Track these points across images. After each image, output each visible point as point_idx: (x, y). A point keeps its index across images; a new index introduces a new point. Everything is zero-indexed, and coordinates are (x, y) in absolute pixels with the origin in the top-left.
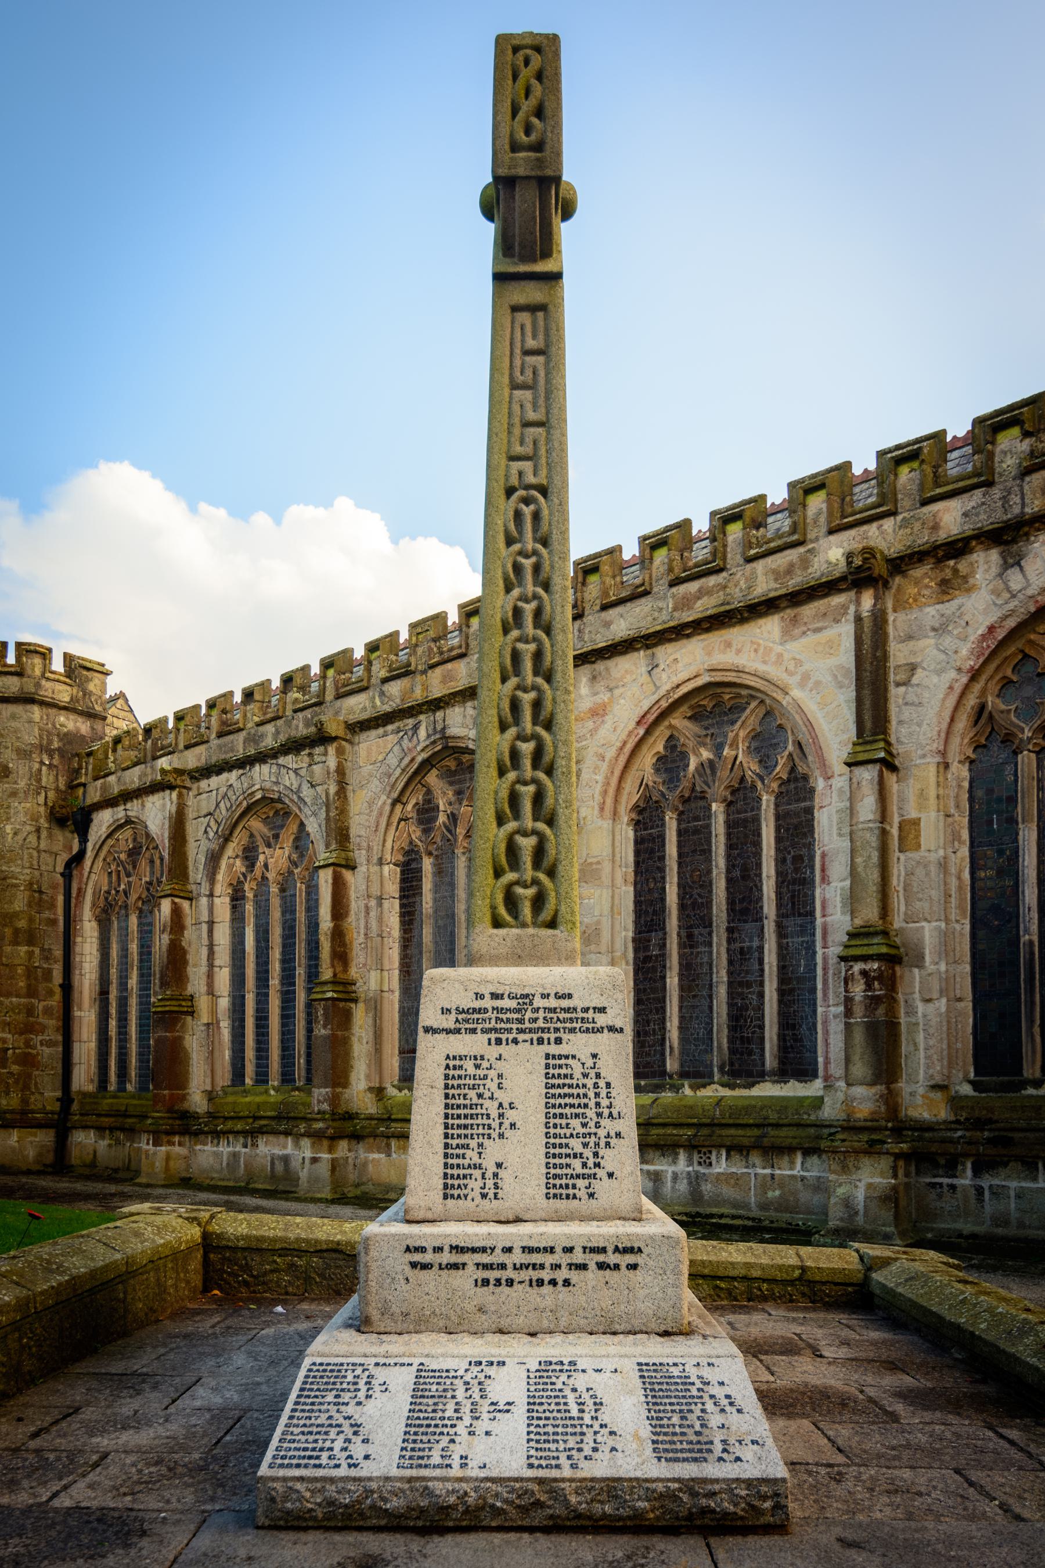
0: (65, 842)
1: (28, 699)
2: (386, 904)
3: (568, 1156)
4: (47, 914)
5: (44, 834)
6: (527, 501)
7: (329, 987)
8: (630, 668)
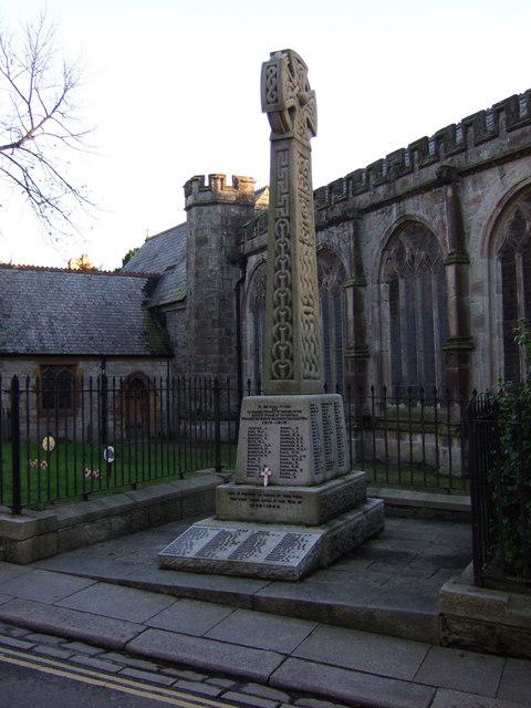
0: (235, 273)
1: (215, 203)
2: (383, 304)
6: (283, 222)
8: (491, 176)
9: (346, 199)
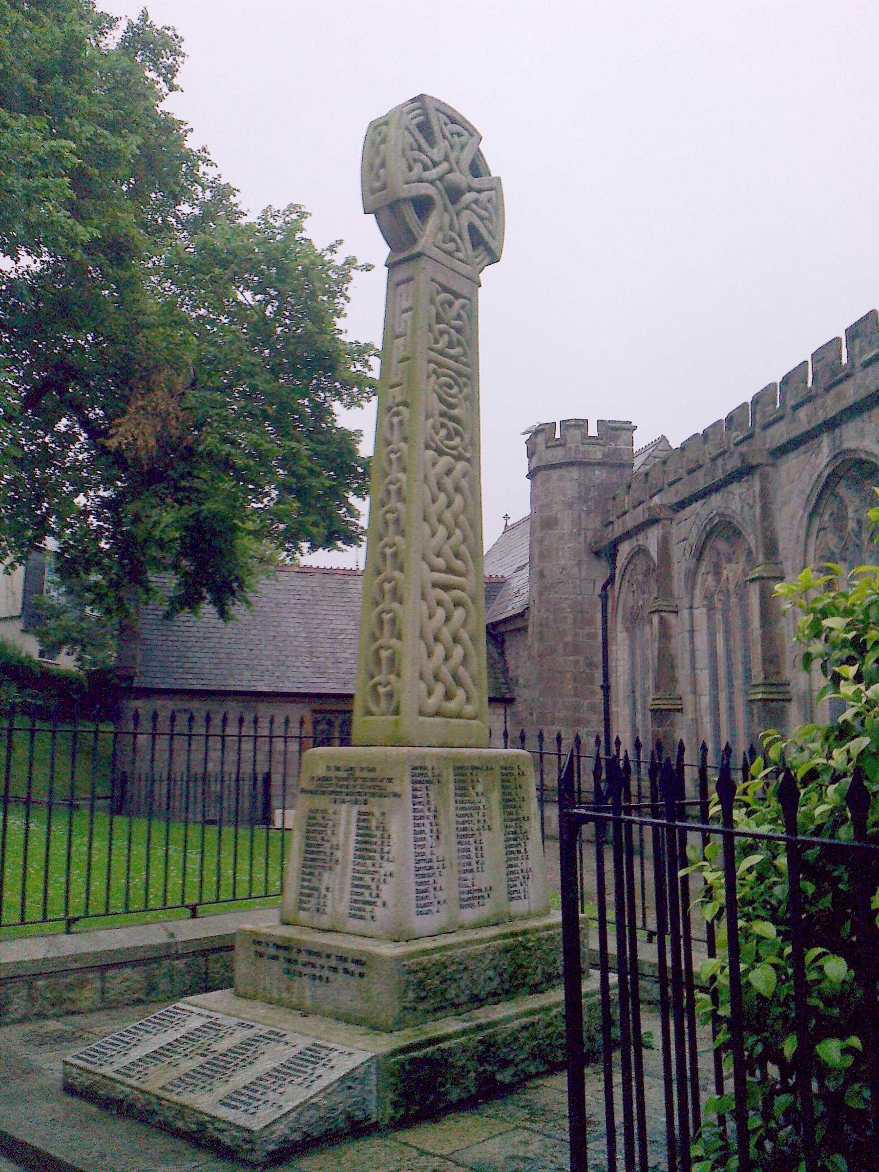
0: (601, 571)
3: (363, 886)
4: (587, 630)
5: (584, 567)
6: (397, 414)
7: (761, 689)
9: (751, 436)
